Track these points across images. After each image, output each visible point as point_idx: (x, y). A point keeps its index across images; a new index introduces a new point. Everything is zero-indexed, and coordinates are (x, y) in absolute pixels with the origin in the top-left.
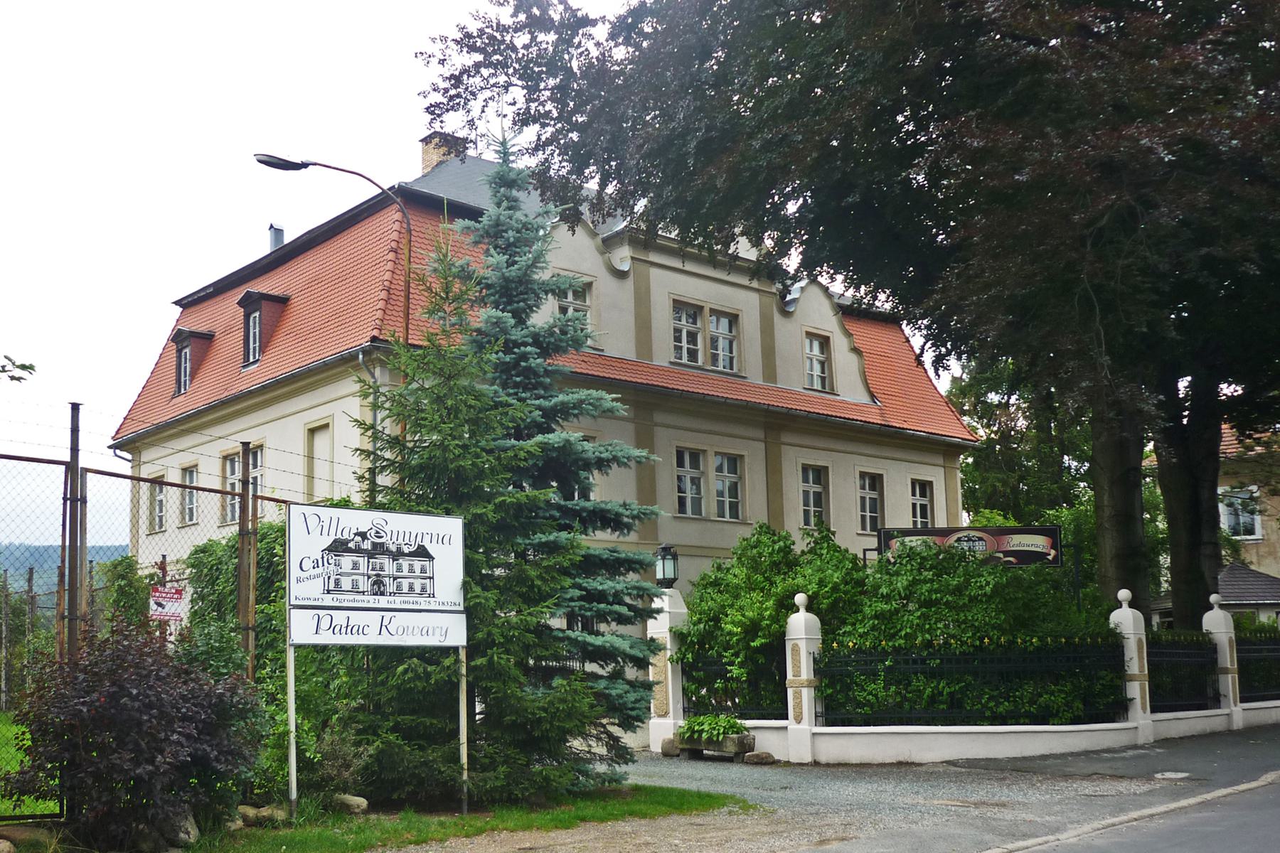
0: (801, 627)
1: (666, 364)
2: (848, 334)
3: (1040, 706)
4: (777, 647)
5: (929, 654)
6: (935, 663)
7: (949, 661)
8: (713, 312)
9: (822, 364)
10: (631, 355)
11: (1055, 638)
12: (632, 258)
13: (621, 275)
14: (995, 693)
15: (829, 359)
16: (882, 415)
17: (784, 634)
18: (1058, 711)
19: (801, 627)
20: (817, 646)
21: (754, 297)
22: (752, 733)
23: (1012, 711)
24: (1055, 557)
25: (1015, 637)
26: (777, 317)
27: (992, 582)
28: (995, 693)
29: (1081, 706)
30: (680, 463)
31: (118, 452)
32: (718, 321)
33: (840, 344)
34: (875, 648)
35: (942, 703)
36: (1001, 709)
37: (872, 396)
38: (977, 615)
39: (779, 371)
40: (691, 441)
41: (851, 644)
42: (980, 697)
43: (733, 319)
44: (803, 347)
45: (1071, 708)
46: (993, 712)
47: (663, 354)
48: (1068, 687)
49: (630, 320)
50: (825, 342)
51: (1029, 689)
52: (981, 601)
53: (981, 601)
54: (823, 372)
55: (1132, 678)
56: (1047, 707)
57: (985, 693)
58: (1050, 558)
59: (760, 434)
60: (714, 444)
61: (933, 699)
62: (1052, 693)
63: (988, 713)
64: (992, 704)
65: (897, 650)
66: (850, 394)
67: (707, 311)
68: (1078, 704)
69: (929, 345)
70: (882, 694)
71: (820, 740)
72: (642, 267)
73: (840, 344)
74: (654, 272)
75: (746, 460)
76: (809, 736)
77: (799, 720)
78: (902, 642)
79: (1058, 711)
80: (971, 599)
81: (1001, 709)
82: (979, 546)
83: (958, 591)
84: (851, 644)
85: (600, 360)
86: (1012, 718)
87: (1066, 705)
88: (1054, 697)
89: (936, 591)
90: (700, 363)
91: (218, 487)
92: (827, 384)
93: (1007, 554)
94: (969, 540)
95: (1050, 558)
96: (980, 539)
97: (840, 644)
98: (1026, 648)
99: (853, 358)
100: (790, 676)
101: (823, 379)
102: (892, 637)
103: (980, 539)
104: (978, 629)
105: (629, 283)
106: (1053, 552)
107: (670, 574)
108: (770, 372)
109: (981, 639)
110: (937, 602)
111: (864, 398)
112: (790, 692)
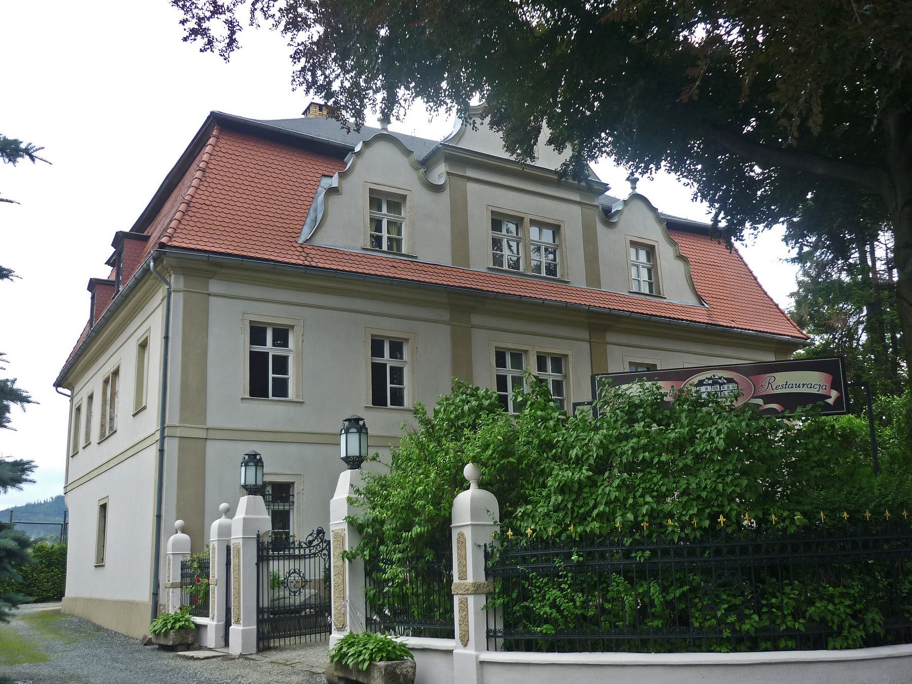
0: (471, 508)
1: (485, 271)
2: (674, 244)
3: (811, 620)
4: (440, 536)
5: (635, 542)
6: (641, 556)
7: (665, 552)
8: (534, 223)
9: (649, 271)
10: (447, 261)
11: (833, 512)
12: (448, 173)
13: (437, 189)
14: (738, 601)
15: (655, 266)
16: (709, 315)
17: (449, 520)
18: (841, 628)
19: (471, 508)
20: (488, 537)
21: (577, 209)
22: (418, 658)
23: (765, 629)
24: (838, 400)
25: (766, 513)
26: (600, 228)
27: (725, 430)
28: (738, 601)
29: (878, 617)
30: (501, 363)
31: (60, 389)
32: (540, 232)
33: (665, 251)
34: (559, 535)
35: (654, 616)
36: (746, 627)
37: (700, 299)
38: (706, 478)
39: (603, 276)
40: (511, 343)
41: (529, 531)
42: (715, 606)
43: (556, 229)
44: (627, 255)
45: (863, 621)
46: (734, 631)
47: (480, 259)
48: (856, 588)
49: (446, 230)
50: (651, 251)
51: (792, 593)
52: (711, 460)
53: (711, 460)
54: (650, 278)
55: (476, 590)
56: (823, 620)
57: (723, 601)
58: (830, 401)
59: (585, 334)
60: (533, 345)
61: (643, 613)
62: (831, 599)
63: (727, 633)
64: (732, 619)
65: (586, 539)
66: (677, 297)
67: (527, 222)
68: (874, 615)
69: (722, 215)
70: (565, 605)
71: (490, 671)
72: (460, 182)
73: (665, 251)
74: (471, 186)
75: (570, 358)
76: (473, 666)
77: (465, 644)
78: (596, 525)
79: (841, 628)
80: (698, 457)
81: (746, 627)
82: (728, 389)
83: (680, 446)
84: (529, 531)
85: (412, 266)
86: (766, 639)
87: (854, 616)
88: (829, 607)
89: (645, 448)
90: (521, 270)
91: (167, 423)
92: (655, 290)
93: (768, 399)
94: (715, 382)
95: (830, 401)
96: (730, 381)
97: (517, 532)
98: (784, 529)
99: (680, 265)
100: (456, 580)
101: (650, 285)
102: (583, 519)
103: (730, 381)
104: (707, 502)
105: (445, 198)
106: (834, 394)
107: (354, 451)
108: (593, 276)
109: (713, 518)
110: (647, 464)
111: (692, 301)
112: (456, 599)
